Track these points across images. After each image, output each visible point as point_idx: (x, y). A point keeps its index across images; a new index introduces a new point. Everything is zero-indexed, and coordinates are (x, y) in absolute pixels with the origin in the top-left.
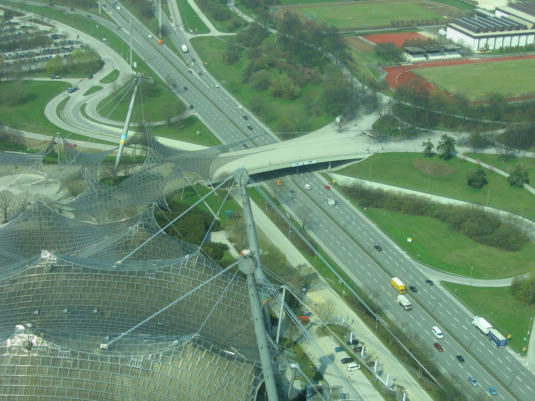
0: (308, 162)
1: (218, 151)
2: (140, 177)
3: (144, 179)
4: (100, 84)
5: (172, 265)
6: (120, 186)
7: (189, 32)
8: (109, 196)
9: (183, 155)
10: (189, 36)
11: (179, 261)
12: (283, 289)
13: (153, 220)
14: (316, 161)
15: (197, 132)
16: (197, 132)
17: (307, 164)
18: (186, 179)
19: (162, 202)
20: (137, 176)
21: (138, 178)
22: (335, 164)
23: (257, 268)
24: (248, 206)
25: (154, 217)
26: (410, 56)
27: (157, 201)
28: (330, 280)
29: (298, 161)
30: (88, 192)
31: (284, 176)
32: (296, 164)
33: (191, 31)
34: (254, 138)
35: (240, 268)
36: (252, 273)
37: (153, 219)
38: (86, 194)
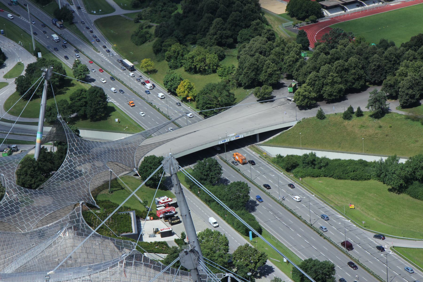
0: (235, 138)
1: (140, 138)
2: (62, 176)
3: (72, 175)
4: (5, 79)
5: (109, 268)
6: (42, 188)
7: (93, 14)
8: (72, 176)
9: (104, 146)
10: (93, 18)
11: (115, 262)
12: (228, 277)
13: (82, 221)
14: (243, 135)
15: (116, 119)
16: (116, 119)
17: (234, 139)
18: (111, 172)
19: (89, 199)
20: (59, 175)
21: (60, 177)
22: (264, 136)
23: (200, 261)
24: (181, 195)
25: (82, 217)
26: (326, 11)
27: (84, 199)
28: (275, 260)
29: (225, 138)
30: (7, 199)
31: (215, 155)
32: (223, 141)
33: (95, 12)
34: (176, 119)
35: (182, 264)
36: (195, 268)
37: (82, 219)
38: (6, 201)
